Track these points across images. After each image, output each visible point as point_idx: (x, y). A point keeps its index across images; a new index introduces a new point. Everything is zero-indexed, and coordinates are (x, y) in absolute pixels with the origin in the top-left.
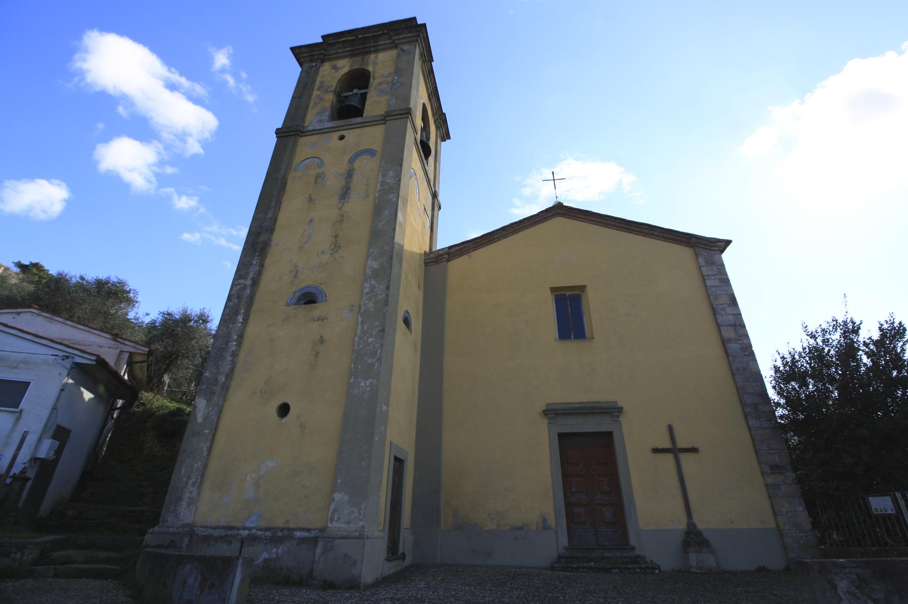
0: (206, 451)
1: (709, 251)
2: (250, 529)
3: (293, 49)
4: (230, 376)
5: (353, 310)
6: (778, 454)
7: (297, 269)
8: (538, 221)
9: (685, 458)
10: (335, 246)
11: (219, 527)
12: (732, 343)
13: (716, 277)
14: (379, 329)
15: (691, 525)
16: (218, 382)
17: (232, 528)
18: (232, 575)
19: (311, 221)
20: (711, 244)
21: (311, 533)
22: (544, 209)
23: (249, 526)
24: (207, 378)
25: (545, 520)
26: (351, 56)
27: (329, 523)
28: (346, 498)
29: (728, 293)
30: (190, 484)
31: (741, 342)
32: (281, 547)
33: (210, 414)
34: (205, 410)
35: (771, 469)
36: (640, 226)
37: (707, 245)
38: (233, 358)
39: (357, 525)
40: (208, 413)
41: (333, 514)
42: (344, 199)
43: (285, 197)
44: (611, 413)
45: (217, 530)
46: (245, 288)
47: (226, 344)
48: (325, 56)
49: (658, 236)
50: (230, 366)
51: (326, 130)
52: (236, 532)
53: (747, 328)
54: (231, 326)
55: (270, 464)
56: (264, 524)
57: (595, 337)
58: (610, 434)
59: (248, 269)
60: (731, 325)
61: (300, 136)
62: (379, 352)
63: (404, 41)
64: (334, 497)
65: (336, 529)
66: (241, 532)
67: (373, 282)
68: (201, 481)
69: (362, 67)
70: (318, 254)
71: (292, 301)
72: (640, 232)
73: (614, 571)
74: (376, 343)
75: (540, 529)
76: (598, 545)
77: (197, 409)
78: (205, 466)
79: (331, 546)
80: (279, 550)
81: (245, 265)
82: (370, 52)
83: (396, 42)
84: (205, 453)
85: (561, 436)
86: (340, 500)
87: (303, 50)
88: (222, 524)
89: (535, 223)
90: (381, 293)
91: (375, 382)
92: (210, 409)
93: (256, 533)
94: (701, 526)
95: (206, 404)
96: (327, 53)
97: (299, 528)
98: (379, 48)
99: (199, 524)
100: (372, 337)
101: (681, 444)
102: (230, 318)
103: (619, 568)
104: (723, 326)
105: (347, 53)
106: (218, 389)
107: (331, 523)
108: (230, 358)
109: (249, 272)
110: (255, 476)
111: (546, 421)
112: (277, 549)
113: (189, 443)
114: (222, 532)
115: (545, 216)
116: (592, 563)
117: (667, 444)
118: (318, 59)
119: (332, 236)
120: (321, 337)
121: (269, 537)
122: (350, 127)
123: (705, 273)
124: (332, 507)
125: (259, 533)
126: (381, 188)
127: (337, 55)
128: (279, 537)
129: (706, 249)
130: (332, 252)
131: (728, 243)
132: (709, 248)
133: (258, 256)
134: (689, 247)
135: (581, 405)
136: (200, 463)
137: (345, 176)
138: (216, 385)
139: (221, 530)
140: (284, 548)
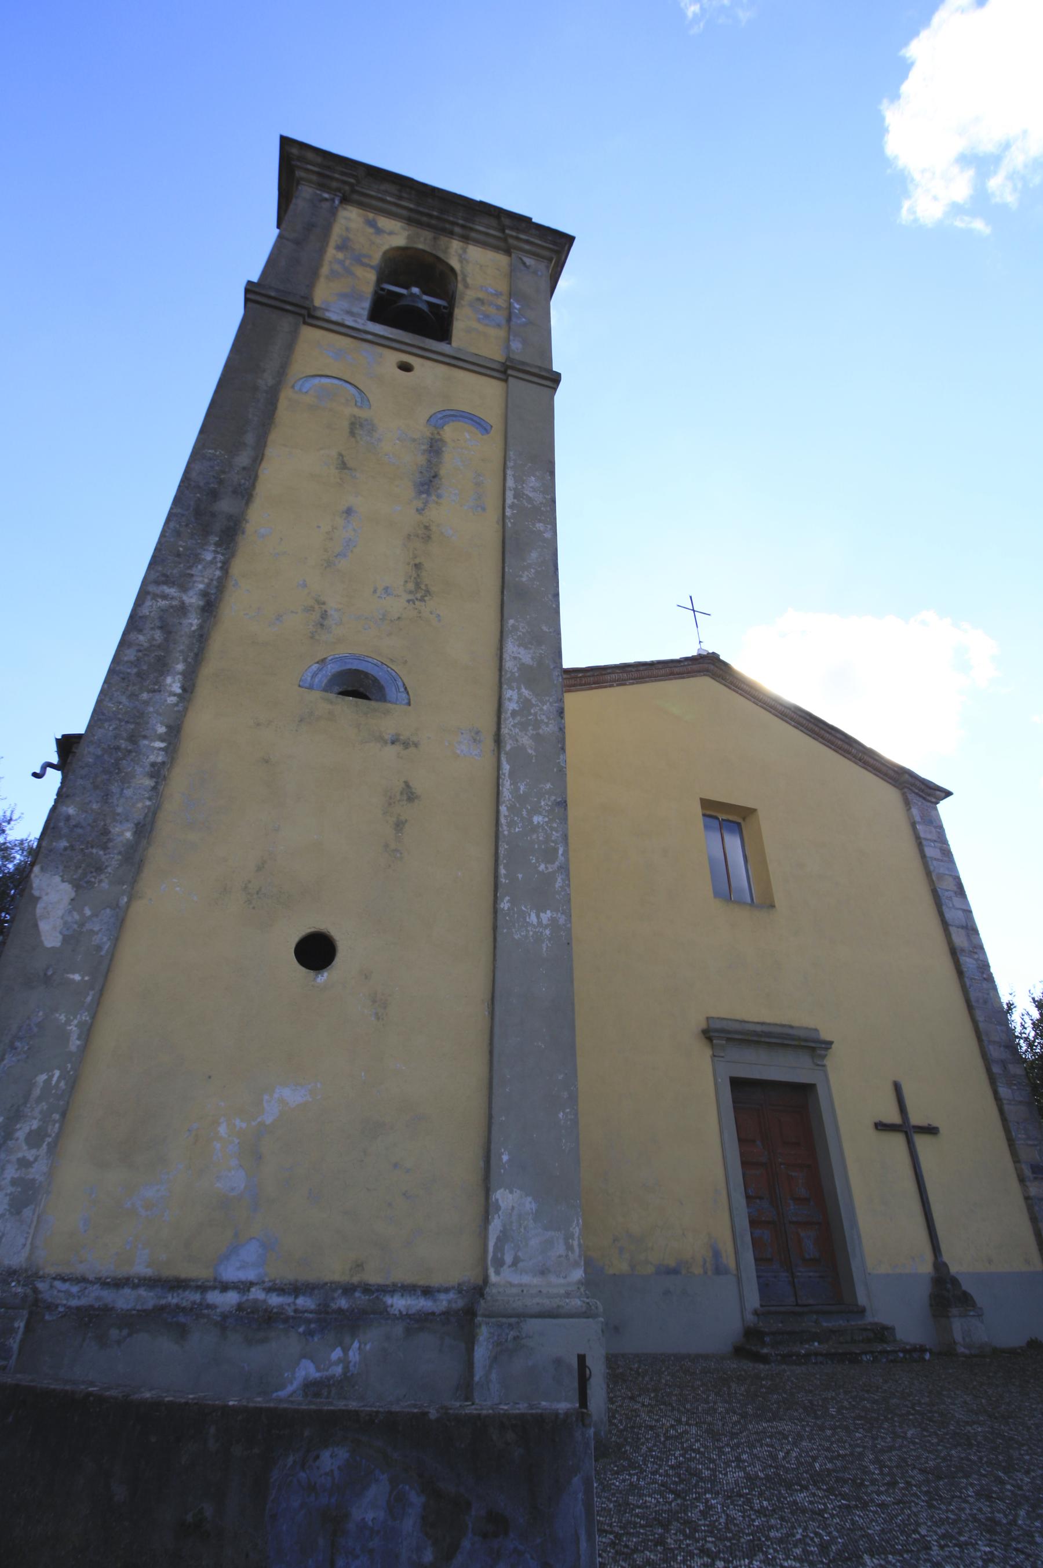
0: (78, 1039)
1: (924, 801)
2: (244, 1287)
3: (286, 142)
4: (144, 830)
5: (480, 742)
6: (1038, 1148)
7: (324, 607)
8: (678, 674)
9: (921, 1142)
10: (418, 585)
11: (128, 1279)
12: (966, 956)
13: (936, 844)
14: (553, 798)
15: (940, 1266)
16: (110, 840)
17: (178, 1284)
18: (576, 1480)
19: (349, 511)
20: (929, 791)
21: (435, 1301)
22: (690, 656)
23: (235, 1280)
24: (73, 822)
25: (716, 1254)
26: (410, 221)
27: (491, 1272)
28: (529, 1205)
29: (953, 874)
30: (20, 1135)
31: (976, 956)
32: (356, 1345)
33: (88, 926)
34: (70, 912)
35: (1034, 1172)
36: (833, 732)
37: (923, 791)
38: (157, 783)
39: (565, 1277)
40: (82, 925)
41: (499, 1247)
42: (428, 493)
43: (274, 437)
44: (813, 1049)
45: (127, 1291)
46: (182, 609)
47: (133, 739)
48: (353, 191)
49: (855, 757)
50: (148, 803)
51: (369, 337)
52: (197, 1297)
53: (981, 936)
54: (145, 696)
55: (292, 1096)
56: (289, 1274)
57: (777, 904)
58: (806, 1090)
59: (190, 568)
60: (962, 927)
61: (305, 323)
62: (560, 852)
63: (527, 247)
64: (497, 1200)
65: (514, 1290)
66: (214, 1297)
67: (526, 692)
68: (61, 1128)
69: (434, 252)
70: (375, 591)
71: (317, 680)
72: (829, 741)
73: (864, 1358)
74: (552, 829)
75: (710, 1273)
76: (797, 1305)
77: (40, 906)
78: (73, 1082)
79: (516, 1338)
80: (351, 1353)
81: (179, 555)
82: (451, 234)
83: (511, 241)
84: (74, 1044)
85: (736, 1083)
86: (513, 1208)
87: (310, 155)
88: (141, 1268)
89: (672, 674)
90: (546, 721)
91: (562, 920)
92: (88, 912)
93: (265, 1301)
94: (954, 1269)
95: (73, 895)
96: (357, 188)
97: (394, 1285)
98: (473, 235)
99: (51, 1270)
100: (541, 814)
101: (915, 1120)
102: (138, 675)
103: (872, 1352)
104: (952, 926)
105: (404, 212)
106: (112, 861)
107: (497, 1273)
108: (149, 782)
109: (192, 575)
110: (244, 1125)
111: (708, 1052)
112: (346, 1350)
113: (718, 1025)
114: (149, 1298)
115: (689, 667)
116: (816, 1344)
117: (895, 1118)
118: (339, 190)
119: (409, 564)
120: (407, 784)
121: (311, 1312)
122: (426, 355)
123: (922, 835)
124: (496, 1226)
125: (275, 1300)
126: (515, 501)
127: (380, 204)
128: (340, 1311)
129: (920, 796)
130: (411, 597)
131: (948, 794)
132: (924, 796)
133: (217, 544)
134: (894, 786)
135: (765, 1029)
136: (57, 1073)
137: (424, 447)
138: (105, 848)
139: (142, 1292)
140: (368, 1347)
